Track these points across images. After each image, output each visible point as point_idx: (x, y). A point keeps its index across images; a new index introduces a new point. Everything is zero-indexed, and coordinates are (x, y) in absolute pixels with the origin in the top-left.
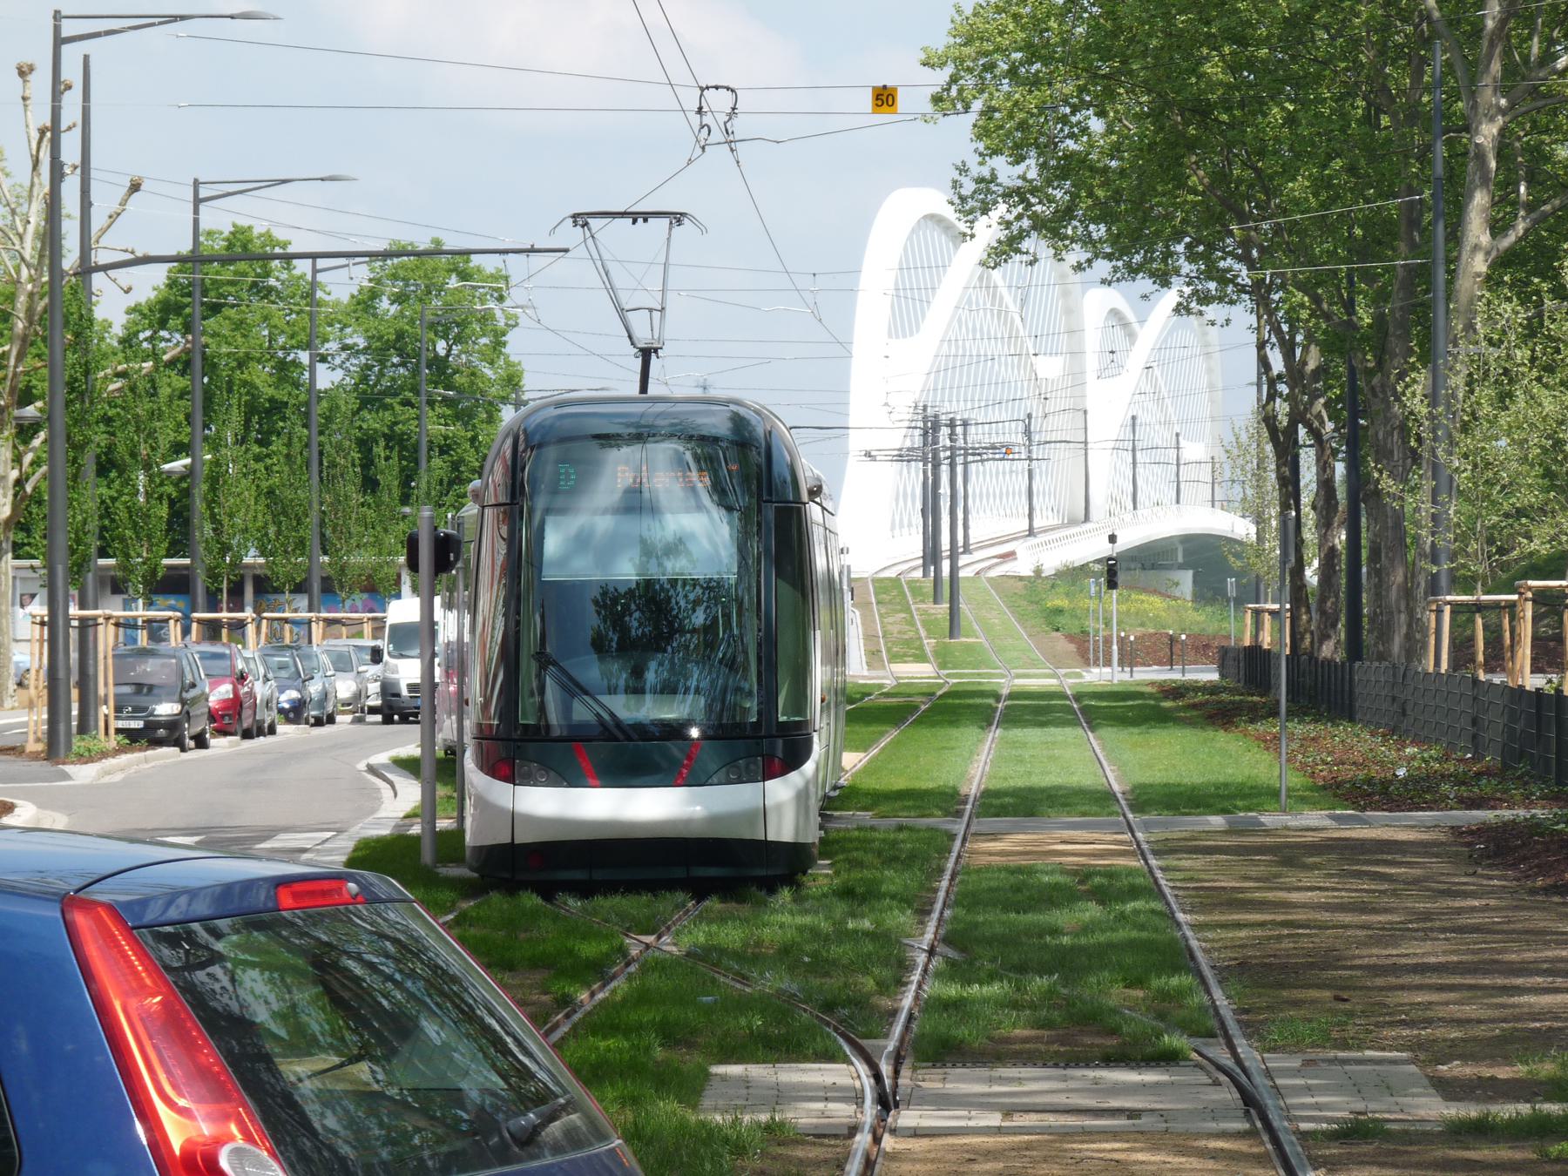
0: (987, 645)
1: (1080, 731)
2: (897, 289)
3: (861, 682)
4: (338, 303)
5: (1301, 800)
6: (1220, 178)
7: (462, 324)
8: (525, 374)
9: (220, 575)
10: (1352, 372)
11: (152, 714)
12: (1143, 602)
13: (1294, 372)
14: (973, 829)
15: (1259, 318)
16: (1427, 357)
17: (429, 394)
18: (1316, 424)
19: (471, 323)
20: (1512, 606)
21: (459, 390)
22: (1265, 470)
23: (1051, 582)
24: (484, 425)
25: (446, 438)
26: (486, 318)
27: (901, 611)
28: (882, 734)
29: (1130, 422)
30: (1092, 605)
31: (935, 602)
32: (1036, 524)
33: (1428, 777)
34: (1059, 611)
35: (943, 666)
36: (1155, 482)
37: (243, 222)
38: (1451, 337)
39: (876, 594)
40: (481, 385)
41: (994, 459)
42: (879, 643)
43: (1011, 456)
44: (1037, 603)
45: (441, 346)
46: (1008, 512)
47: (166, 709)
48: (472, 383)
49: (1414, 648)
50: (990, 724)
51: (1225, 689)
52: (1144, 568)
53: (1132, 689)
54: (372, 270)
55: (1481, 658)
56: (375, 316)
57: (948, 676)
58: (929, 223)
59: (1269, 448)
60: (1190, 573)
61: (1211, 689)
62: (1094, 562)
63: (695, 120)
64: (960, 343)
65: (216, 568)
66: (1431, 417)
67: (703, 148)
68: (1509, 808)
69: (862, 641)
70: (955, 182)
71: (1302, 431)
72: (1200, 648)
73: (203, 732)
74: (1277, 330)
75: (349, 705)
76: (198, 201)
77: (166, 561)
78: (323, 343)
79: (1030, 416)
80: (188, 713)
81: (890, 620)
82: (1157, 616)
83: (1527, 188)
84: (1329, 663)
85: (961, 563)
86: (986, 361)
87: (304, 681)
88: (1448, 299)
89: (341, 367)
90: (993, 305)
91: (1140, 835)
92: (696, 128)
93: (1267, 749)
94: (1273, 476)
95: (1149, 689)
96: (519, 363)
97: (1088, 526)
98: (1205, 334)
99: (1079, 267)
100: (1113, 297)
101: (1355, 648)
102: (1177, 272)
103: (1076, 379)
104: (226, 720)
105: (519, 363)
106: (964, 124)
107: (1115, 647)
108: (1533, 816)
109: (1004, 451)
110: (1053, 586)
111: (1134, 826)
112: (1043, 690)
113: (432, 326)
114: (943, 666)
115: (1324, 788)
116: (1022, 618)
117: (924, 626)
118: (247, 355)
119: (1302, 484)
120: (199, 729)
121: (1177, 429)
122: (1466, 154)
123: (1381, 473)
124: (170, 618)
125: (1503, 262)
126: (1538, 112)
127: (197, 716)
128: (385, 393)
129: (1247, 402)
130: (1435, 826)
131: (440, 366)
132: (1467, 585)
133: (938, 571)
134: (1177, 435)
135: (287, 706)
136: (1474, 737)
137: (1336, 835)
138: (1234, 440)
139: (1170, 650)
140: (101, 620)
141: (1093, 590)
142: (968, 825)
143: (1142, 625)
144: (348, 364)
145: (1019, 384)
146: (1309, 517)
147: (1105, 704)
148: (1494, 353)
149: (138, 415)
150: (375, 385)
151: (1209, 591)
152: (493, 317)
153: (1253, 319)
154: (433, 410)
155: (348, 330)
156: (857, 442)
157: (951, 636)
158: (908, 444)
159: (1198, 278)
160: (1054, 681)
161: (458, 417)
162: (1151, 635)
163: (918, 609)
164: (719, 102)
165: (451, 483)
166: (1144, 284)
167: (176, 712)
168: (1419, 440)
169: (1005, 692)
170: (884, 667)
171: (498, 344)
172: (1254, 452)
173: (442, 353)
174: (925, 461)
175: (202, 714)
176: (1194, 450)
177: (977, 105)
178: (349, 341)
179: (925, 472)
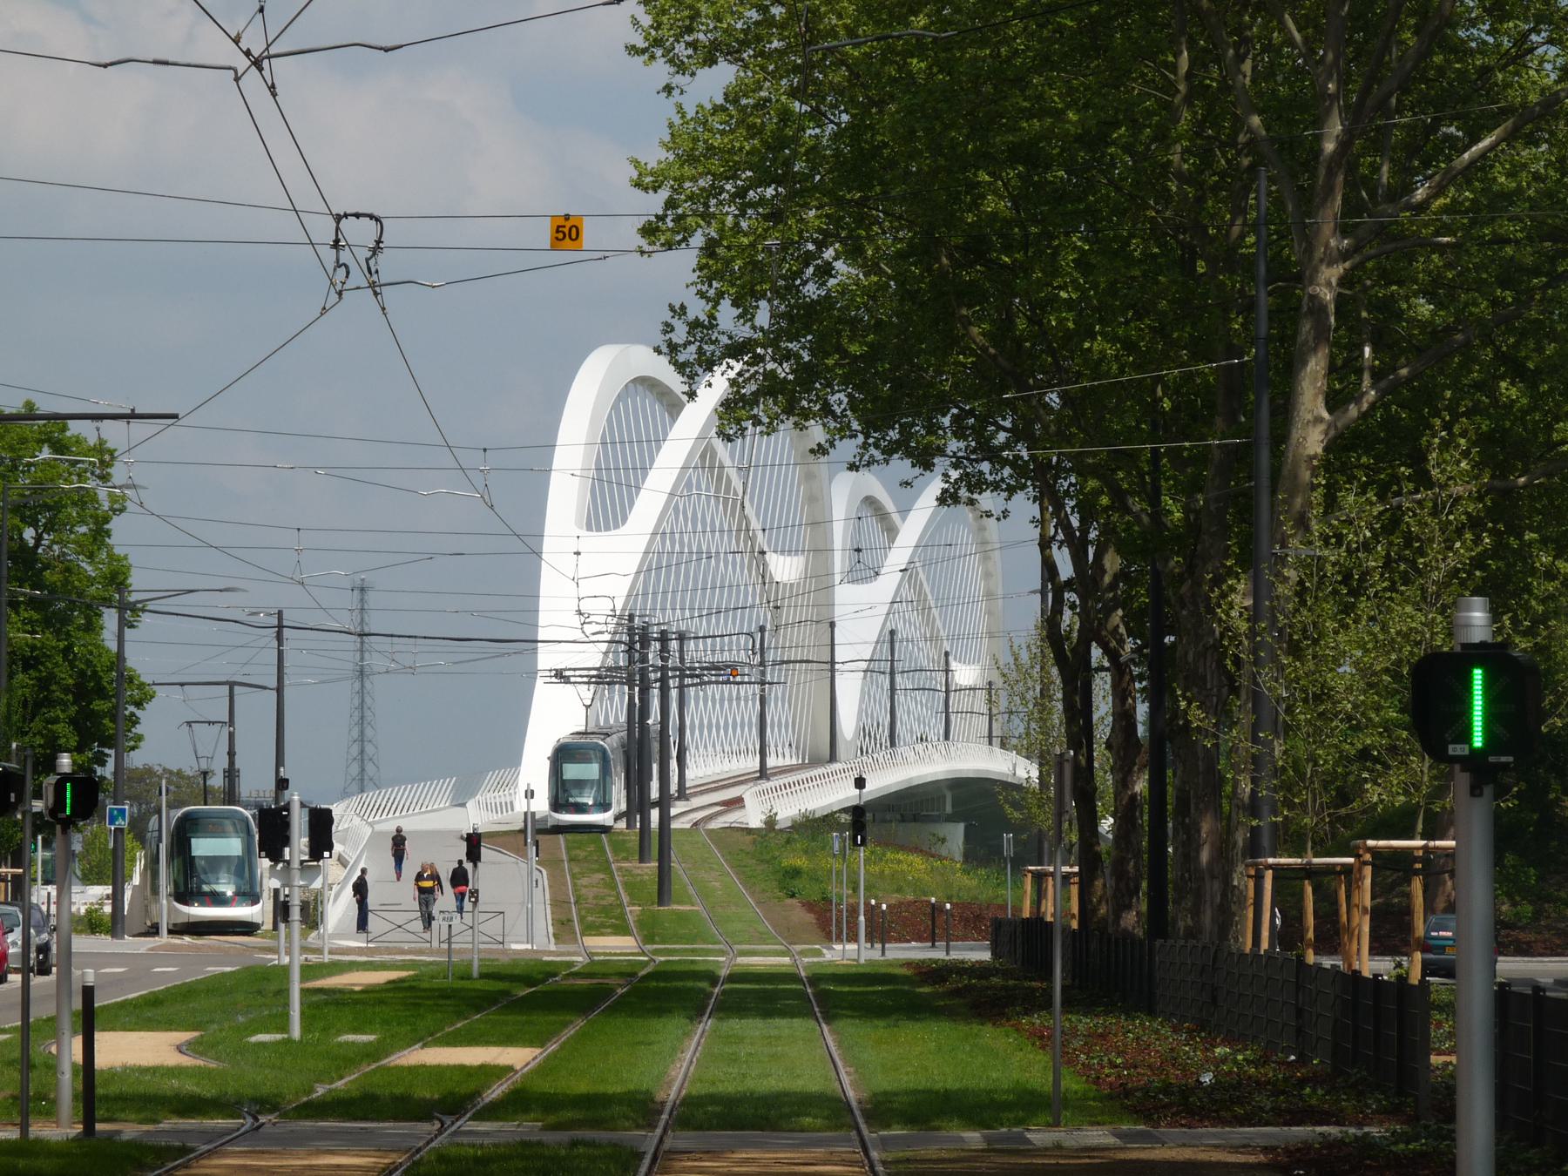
1: (812, 1023)
2: (598, 469)
3: (545, 958)
5: (1084, 1111)
6: (1002, 330)
7: (57, 508)
8: (133, 572)
10: (1156, 574)
12: (899, 862)
13: (1086, 580)
14: (667, 1145)
15: (1043, 509)
16: (1248, 560)
17: (13, 594)
18: (1113, 644)
19: (65, 506)
20: (1347, 869)
21: (53, 591)
22: (1051, 699)
24: (81, 634)
25: (33, 648)
26: (85, 500)
27: (598, 871)
28: (565, 1025)
29: (888, 638)
30: (836, 865)
31: (642, 860)
32: (771, 762)
33: (1239, 1082)
34: (796, 873)
35: (649, 939)
36: (916, 711)
38: (1279, 536)
39: (567, 853)
41: (717, 683)
42: (570, 911)
43: (738, 679)
45: (29, 534)
46: (735, 747)
48: (66, 582)
49: (1226, 919)
50: (702, 1015)
51: (997, 970)
52: (903, 820)
53: (883, 970)
55: (1311, 935)
57: (656, 952)
58: (640, 388)
59: (1055, 671)
60: (961, 827)
61: (978, 970)
62: (840, 811)
63: (329, 255)
64: (677, 536)
66: (1252, 633)
67: (340, 294)
68: (1337, 1124)
69: (548, 907)
71: (1096, 653)
72: (970, 920)
74: (1064, 524)
79: (762, 629)
81: (584, 881)
83: (1374, 351)
84: (1127, 935)
85: (673, 812)
86: (709, 558)
88: (1274, 492)
90: (717, 490)
91: (875, 1154)
92: (330, 266)
93: (1043, 1047)
94: (1060, 706)
95: (903, 971)
96: (126, 557)
97: (836, 766)
98: (982, 529)
100: (871, 482)
101: (1158, 921)
102: (941, 451)
103: (819, 583)
105: (126, 557)
106: (682, 263)
107: (862, 918)
108: (1367, 1134)
109: (726, 672)
110: (788, 842)
111: (869, 1145)
112: (773, 970)
113: (18, 509)
114: (649, 939)
115: (1110, 1097)
116: (748, 881)
119: (1095, 717)
121: (946, 646)
122: (1298, 309)
123: (1189, 703)
125: (1341, 446)
126: (1387, 258)
129: (1030, 611)
130: (1244, 1146)
132: (1292, 840)
133: (645, 821)
134: (947, 654)
136: (1299, 1031)
137: (1121, 1156)
138: (1012, 661)
139: (931, 924)
141: (837, 846)
142: (661, 1141)
143: (899, 890)
145: (750, 589)
146: (1101, 756)
147: (846, 989)
148: (1331, 555)
151: (981, 852)
153: (1035, 510)
154: (17, 613)
156: (547, 658)
157: (661, 902)
158: (610, 662)
159: (968, 459)
160: (787, 960)
161: (47, 623)
162: (910, 904)
163: (620, 869)
164: (359, 233)
165: (38, 705)
166: (901, 467)
168: (1237, 661)
169: (723, 972)
171: (100, 533)
172: (1036, 676)
173: (31, 543)
174: (630, 682)
176: (966, 674)
177: (698, 240)
179: (631, 698)
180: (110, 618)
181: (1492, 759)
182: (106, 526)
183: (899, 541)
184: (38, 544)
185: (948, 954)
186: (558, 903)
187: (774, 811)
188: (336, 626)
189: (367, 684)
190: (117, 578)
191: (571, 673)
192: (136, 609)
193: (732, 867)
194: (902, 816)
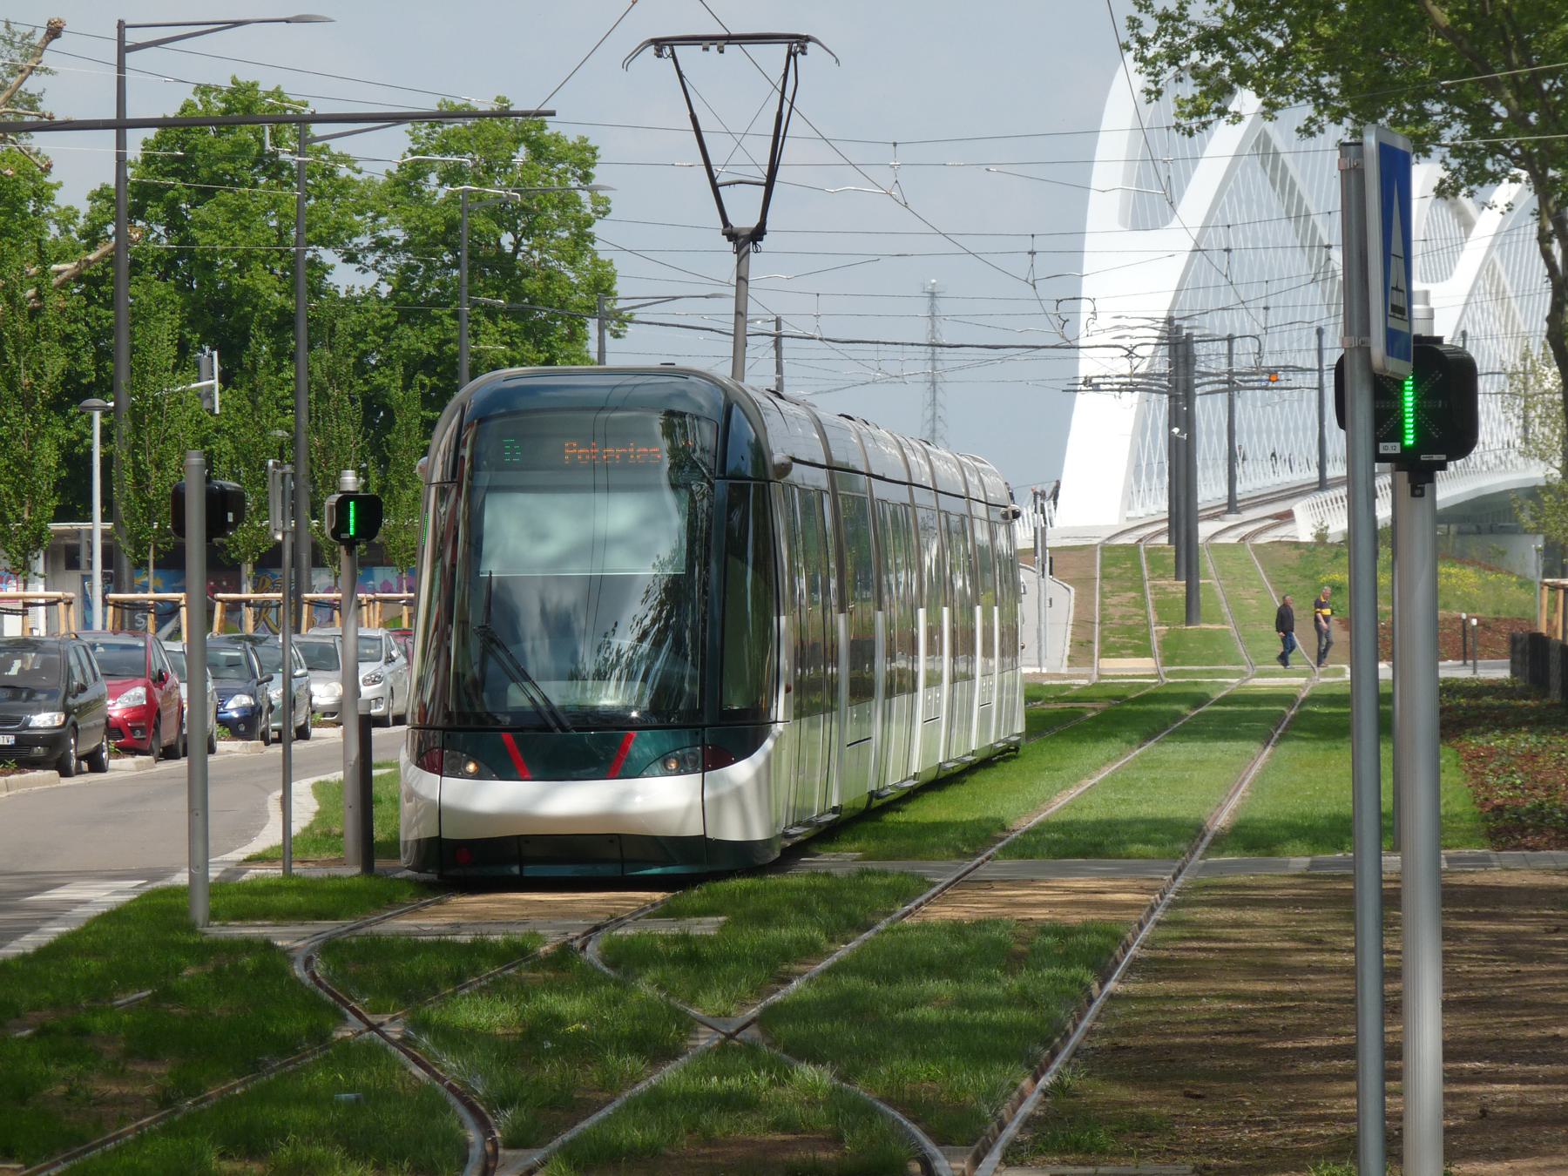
0: (1234, 634)
3: (1048, 682)
4: (371, 183)
8: (618, 280)
9: (145, 542)
11: (26, 727)
23: (1334, 550)
24: (564, 344)
27: (1130, 589)
37: (245, 77)
39: (1103, 567)
40: (559, 291)
42: (1093, 632)
44: (1311, 577)
45: (507, 240)
47: (44, 720)
52: (1479, 532)
54: (415, 140)
56: (419, 199)
61: (1493, 688)
65: (139, 533)
69: (1070, 628)
70: (1132, 20)
73: (99, 749)
75: (333, 714)
76: (123, 49)
77: (54, 526)
78: (350, 237)
80: (74, 725)
81: (1114, 600)
82: (1468, 594)
87: (260, 683)
89: (375, 268)
96: (610, 263)
99: (1306, 131)
104: (138, 735)
105: (610, 263)
114: (1168, 661)
117: (1156, 608)
118: (248, 253)
120: (94, 745)
124: (59, 600)
127: (88, 729)
128: (435, 302)
131: (505, 264)
135: (235, 715)
140: (365, 602)
144: (384, 265)
147: (1326, 710)
149: (17, 332)
150: (420, 291)
152: (576, 202)
154: (495, 324)
155: (383, 220)
157: (1189, 621)
163: (1154, 587)
167: (57, 724)
170: (1092, 662)
171: (582, 238)
173: (509, 249)
175: (96, 726)
178: (385, 234)
180: (592, 326)
181: (1423, 458)
182: (589, 230)
183: (1476, 232)
184: (517, 249)
185: (1475, 672)
186: (1081, 623)
187: (1325, 524)
188: (800, 333)
189: (939, 396)
190: (601, 286)
191: (1101, 380)
192: (623, 321)
193: (1272, 583)
194: (1478, 527)
